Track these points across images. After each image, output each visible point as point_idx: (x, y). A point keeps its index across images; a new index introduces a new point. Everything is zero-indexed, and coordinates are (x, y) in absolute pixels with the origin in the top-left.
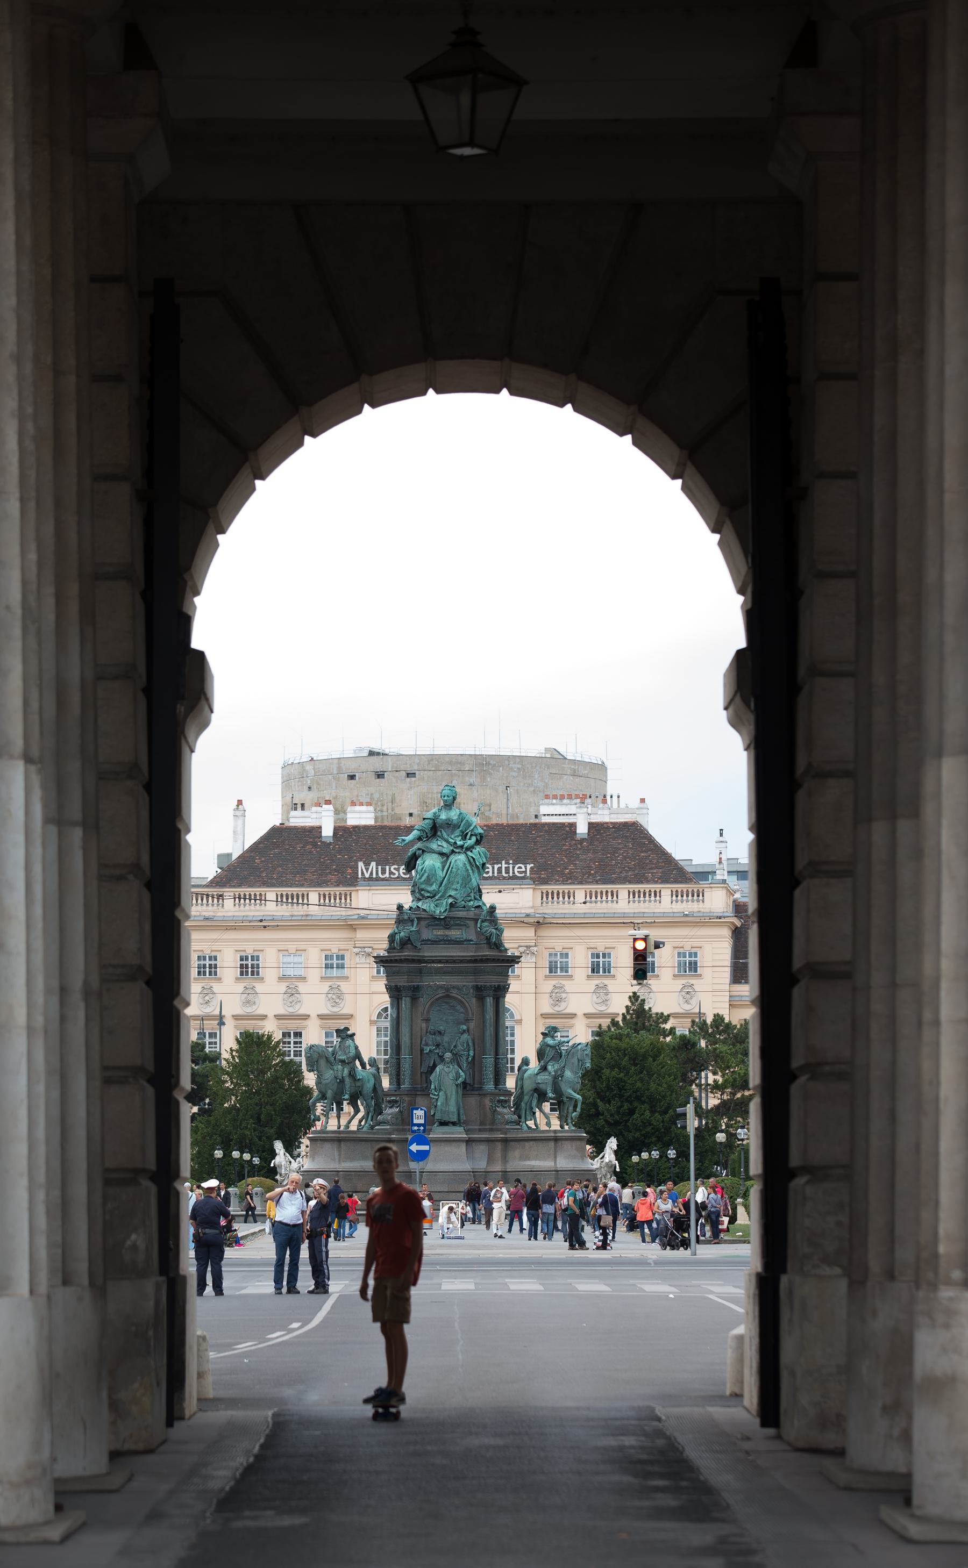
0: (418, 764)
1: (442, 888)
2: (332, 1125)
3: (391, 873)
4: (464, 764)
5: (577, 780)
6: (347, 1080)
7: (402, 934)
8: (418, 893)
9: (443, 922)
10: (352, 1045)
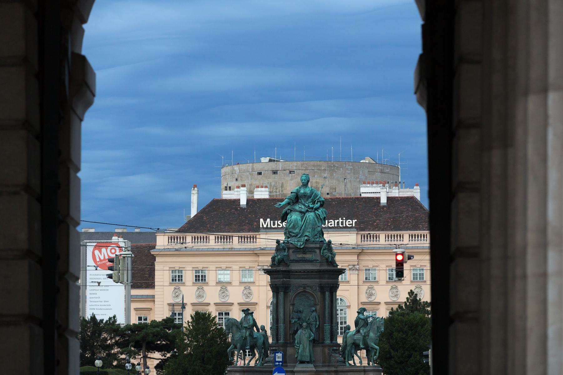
0: (296, 166)
1: (301, 231)
2: (240, 363)
3: (278, 225)
4: (321, 166)
5: (383, 175)
6: (248, 338)
7: (279, 257)
8: (288, 233)
9: (302, 250)
10: (251, 318)
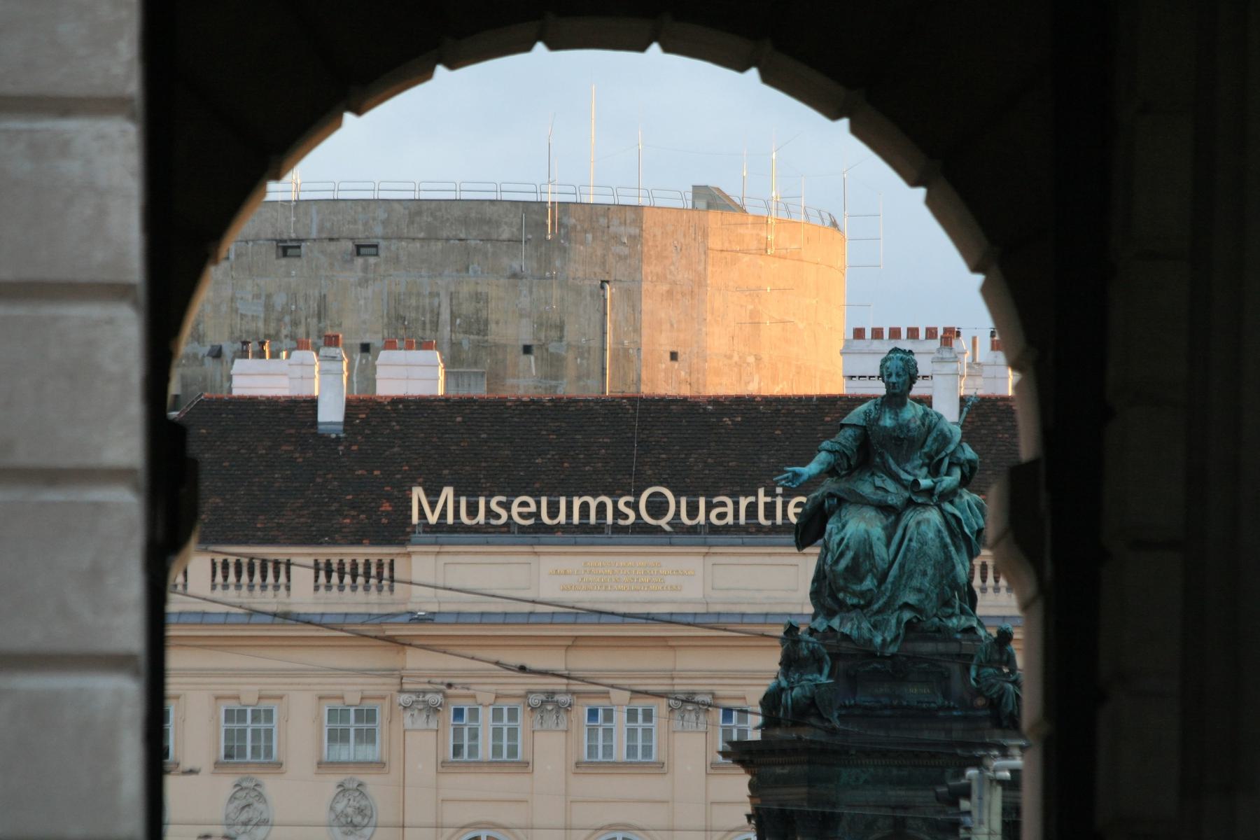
0: (385, 223)
3: (490, 513)
7: (797, 691)
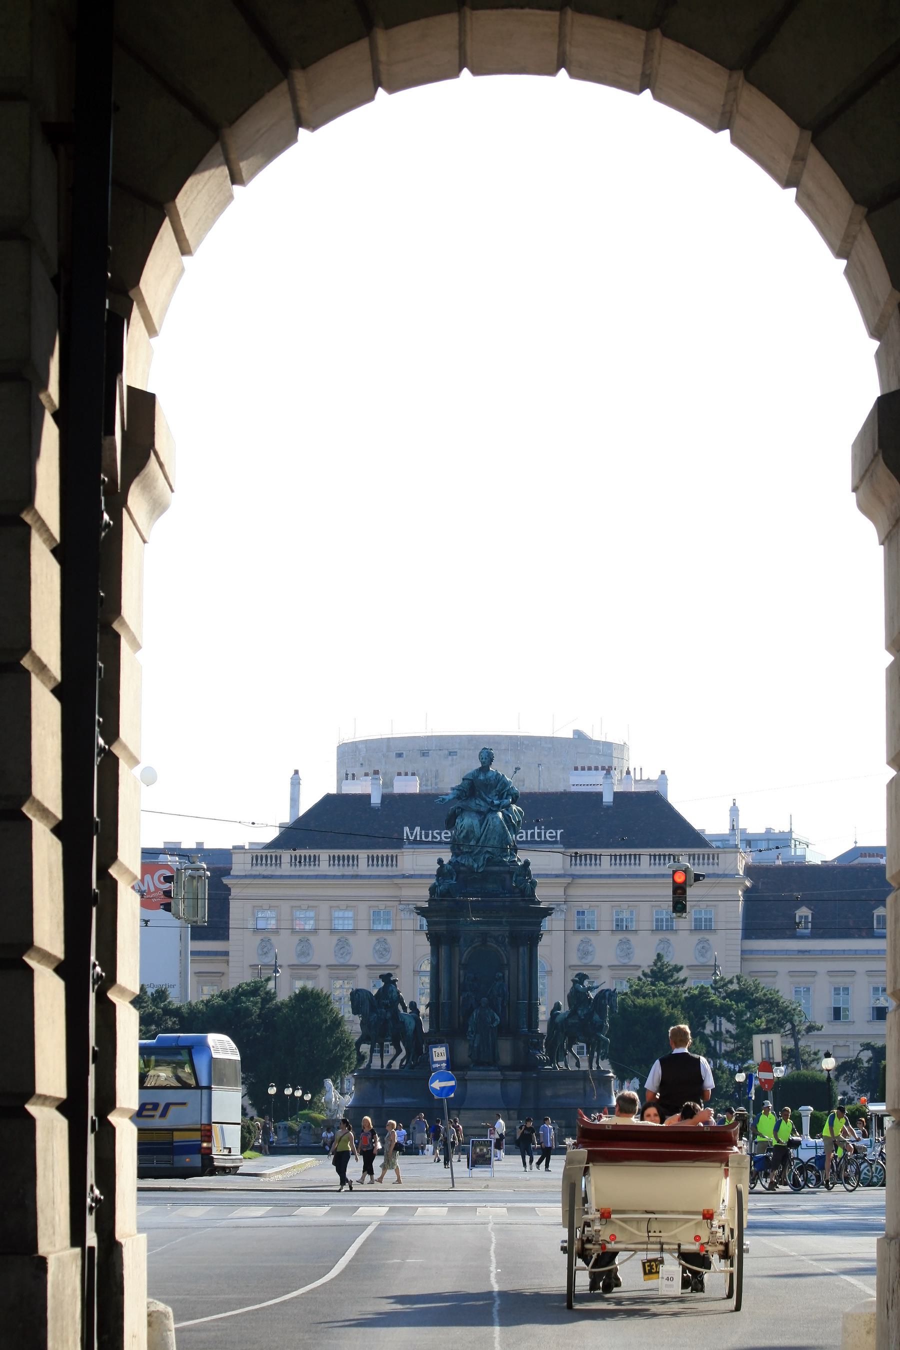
2: (376, 1064)
3: (433, 837)
8: (455, 846)
